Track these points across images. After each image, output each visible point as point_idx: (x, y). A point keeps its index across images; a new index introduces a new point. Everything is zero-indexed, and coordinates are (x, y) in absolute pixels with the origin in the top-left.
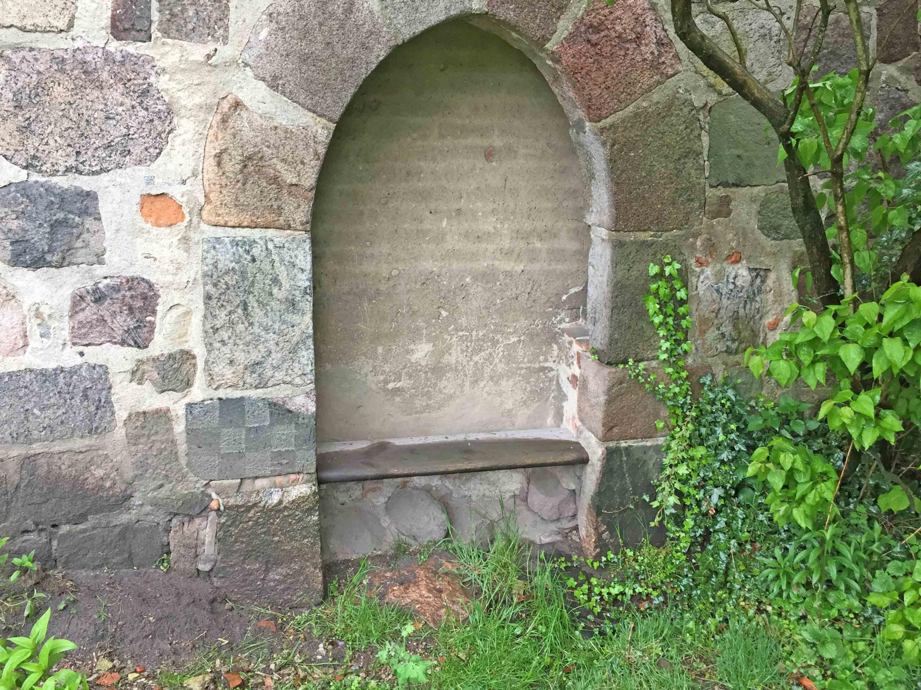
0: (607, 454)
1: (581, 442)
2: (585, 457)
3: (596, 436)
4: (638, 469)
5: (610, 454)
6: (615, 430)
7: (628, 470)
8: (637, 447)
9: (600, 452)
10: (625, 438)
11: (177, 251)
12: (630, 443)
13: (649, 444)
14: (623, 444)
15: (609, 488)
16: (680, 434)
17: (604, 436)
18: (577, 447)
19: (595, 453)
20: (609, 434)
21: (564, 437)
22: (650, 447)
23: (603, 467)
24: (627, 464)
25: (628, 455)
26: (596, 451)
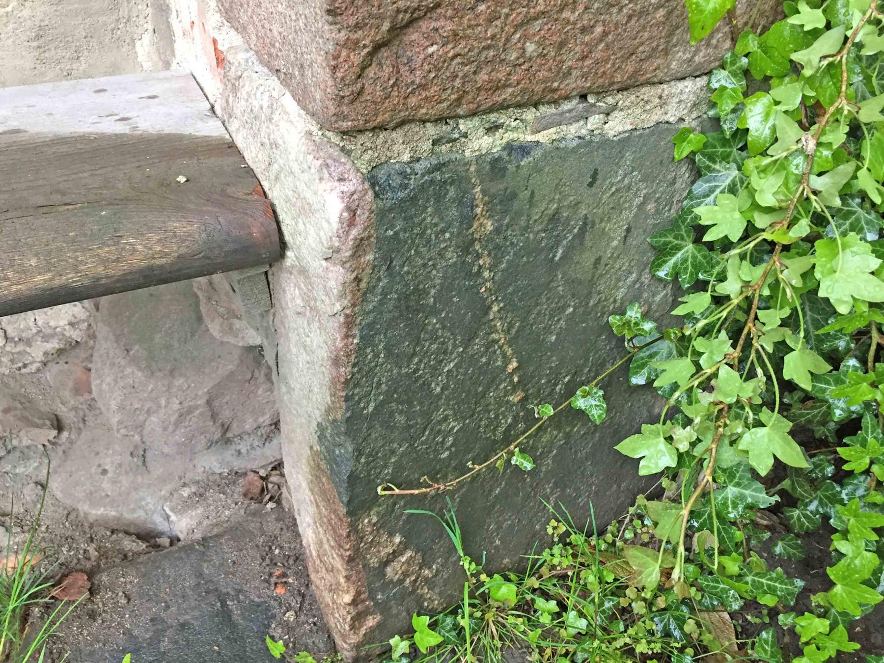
0: (382, 216)
1: (810, 10)
2: (257, 229)
3: (302, 99)
4: (552, 266)
5: (397, 222)
6: (424, 47)
7: (499, 287)
8: (558, 152)
9: (333, 208)
10: (489, 108)
11: (497, 136)
12: (522, 129)
13: (617, 126)
14: (480, 142)
15: (410, 390)
16: (827, 44)
17: (350, 93)
18: (215, 170)
19: (306, 210)
20: (381, 72)
21: (156, 118)
22: (625, 141)
23: (359, 290)
24: (497, 252)
25: (503, 203)
26: (315, 201)
